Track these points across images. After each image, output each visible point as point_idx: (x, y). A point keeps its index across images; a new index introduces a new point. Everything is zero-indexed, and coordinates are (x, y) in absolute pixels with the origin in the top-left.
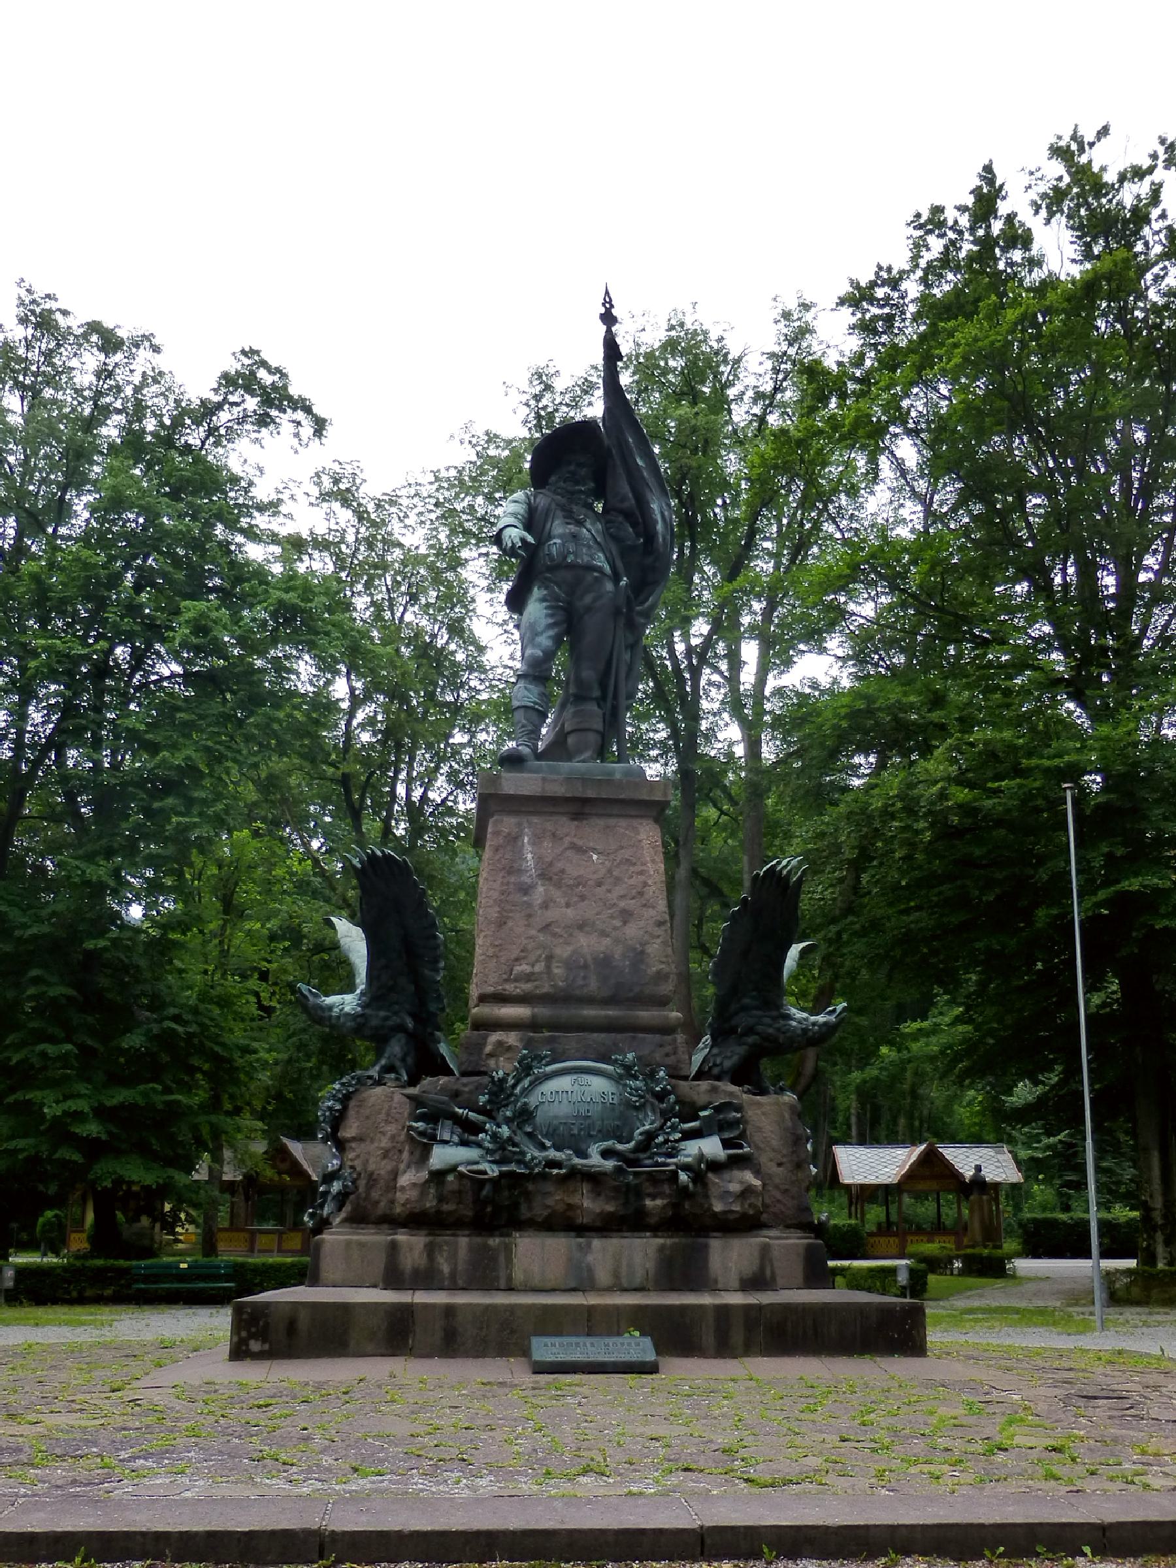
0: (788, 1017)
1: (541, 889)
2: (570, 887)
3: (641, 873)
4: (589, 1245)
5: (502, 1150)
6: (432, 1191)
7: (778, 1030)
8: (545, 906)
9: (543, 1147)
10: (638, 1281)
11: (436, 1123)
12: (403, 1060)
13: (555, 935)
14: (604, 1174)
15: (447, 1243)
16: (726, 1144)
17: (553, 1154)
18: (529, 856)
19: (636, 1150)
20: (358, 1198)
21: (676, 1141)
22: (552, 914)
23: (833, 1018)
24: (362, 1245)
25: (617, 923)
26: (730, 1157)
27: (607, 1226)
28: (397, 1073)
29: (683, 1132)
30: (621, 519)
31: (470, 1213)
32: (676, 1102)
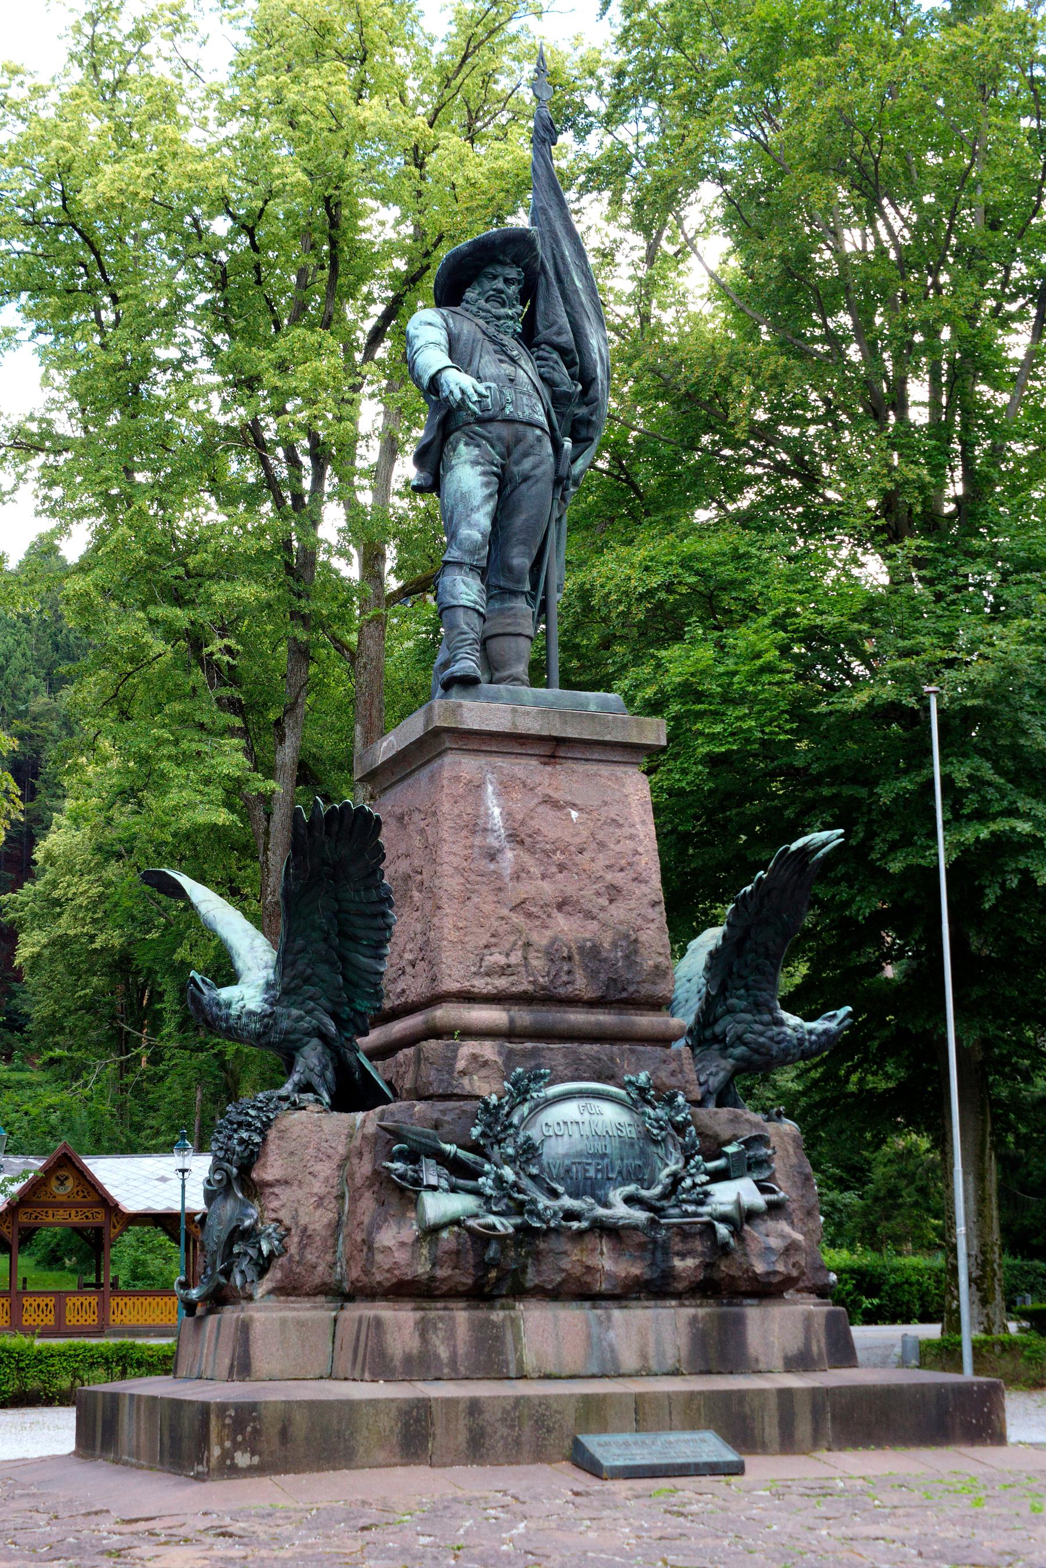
0: (780, 1023)
1: (509, 855)
3: (632, 837)
4: (609, 1318)
6: (425, 1251)
7: (771, 1039)
8: (517, 877)
9: (554, 1194)
10: (670, 1363)
12: (322, 1075)
13: (529, 915)
14: (635, 1228)
15: (441, 1319)
18: (496, 811)
20: (291, 1259)
22: (525, 889)
23: (833, 1025)
24: (301, 1324)
25: (604, 901)
27: (627, 1293)
28: (315, 1092)
29: (707, 1172)
30: (555, 356)
31: (470, 1281)
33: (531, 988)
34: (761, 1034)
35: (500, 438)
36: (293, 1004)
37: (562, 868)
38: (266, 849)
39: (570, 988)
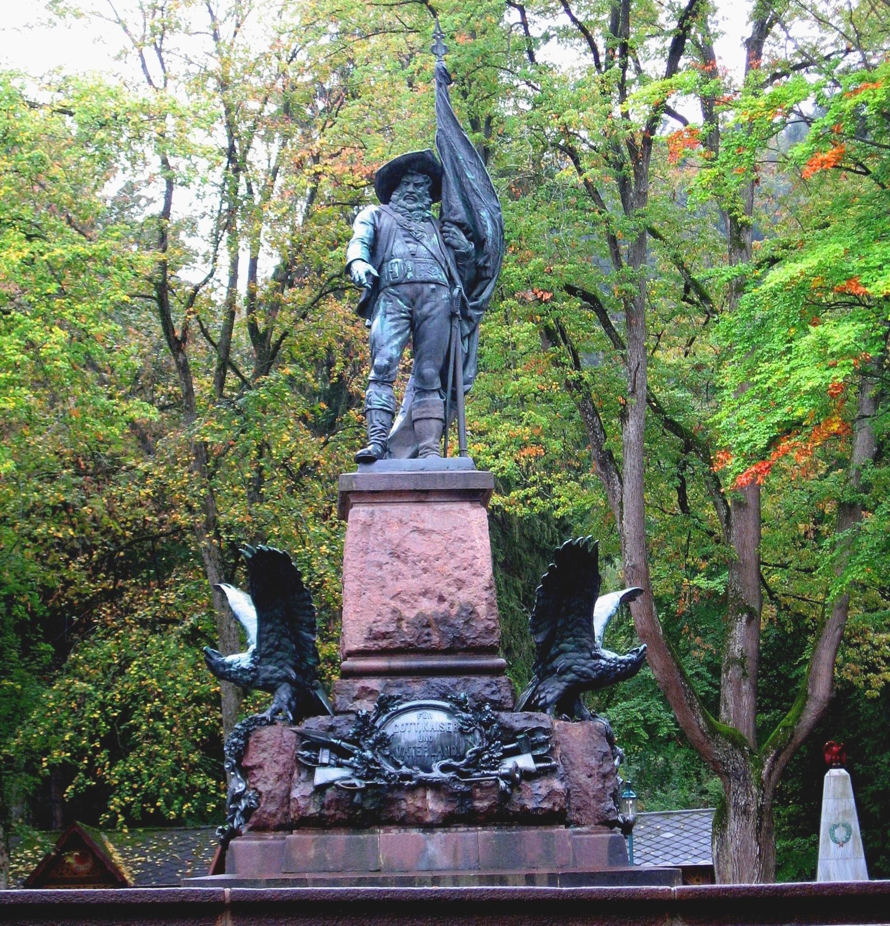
0: (599, 657)
2: (414, 562)
3: (472, 548)
5: (370, 770)
7: (591, 668)
9: (398, 766)
11: (318, 751)
13: (404, 601)
16: (537, 759)
17: (405, 770)
19: (467, 766)
21: (498, 758)
22: (400, 585)
23: (634, 656)
25: (453, 589)
26: (539, 769)
27: (447, 821)
29: (504, 751)
32: (498, 729)
33: (403, 645)
34: (584, 665)
35: (406, 295)
36: (270, 663)
37: (425, 570)
38: (621, 519)
39: (428, 644)
